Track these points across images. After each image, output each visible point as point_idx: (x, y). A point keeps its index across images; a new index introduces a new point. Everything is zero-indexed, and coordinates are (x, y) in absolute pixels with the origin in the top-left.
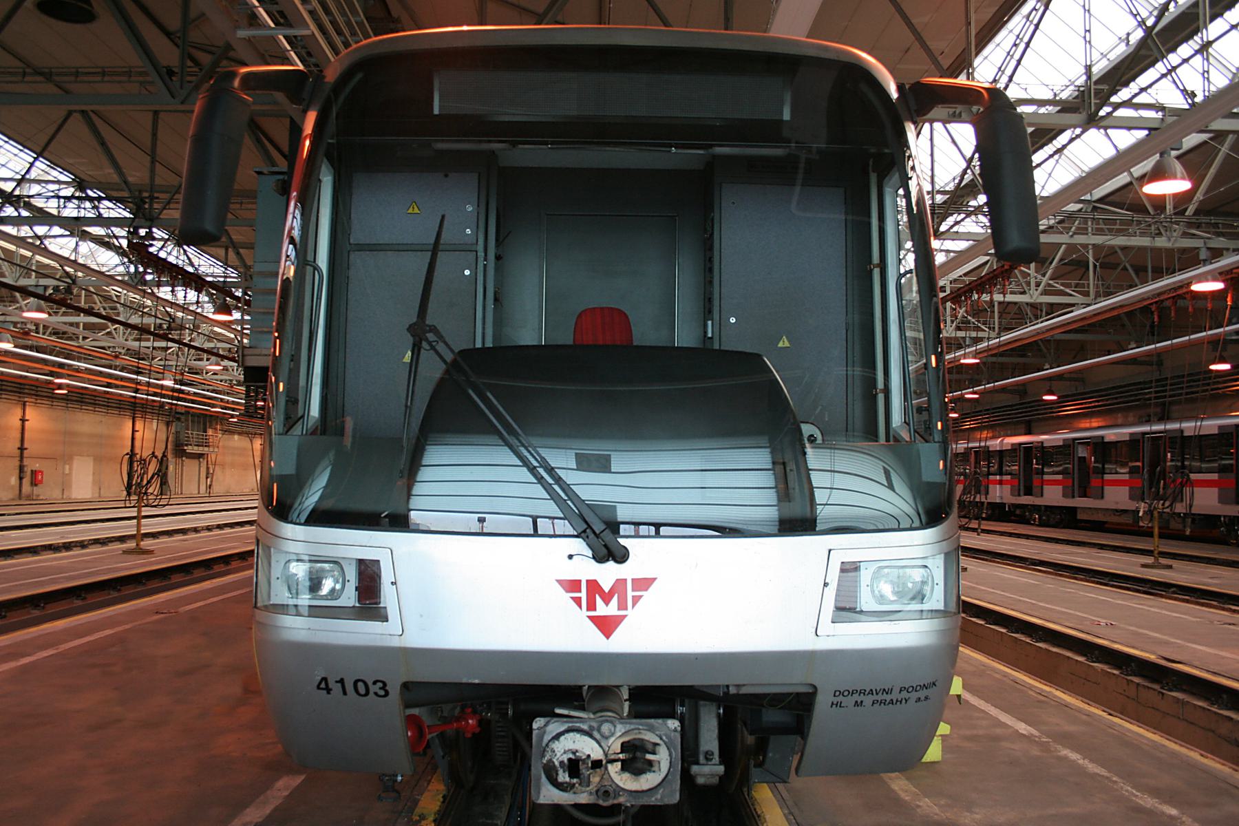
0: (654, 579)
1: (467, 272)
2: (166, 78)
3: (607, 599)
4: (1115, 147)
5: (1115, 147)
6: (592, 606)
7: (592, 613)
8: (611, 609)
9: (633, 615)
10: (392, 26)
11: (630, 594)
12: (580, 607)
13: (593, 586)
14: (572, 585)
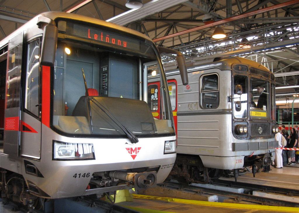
0: (43, 177)
2: (290, 166)
3: (134, 152)
6: (131, 153)
7: (132, 155)
10: (293, 84)
11: (137, 150)
12: (129, 153)
13: (132, 149)
14: (128, 149)
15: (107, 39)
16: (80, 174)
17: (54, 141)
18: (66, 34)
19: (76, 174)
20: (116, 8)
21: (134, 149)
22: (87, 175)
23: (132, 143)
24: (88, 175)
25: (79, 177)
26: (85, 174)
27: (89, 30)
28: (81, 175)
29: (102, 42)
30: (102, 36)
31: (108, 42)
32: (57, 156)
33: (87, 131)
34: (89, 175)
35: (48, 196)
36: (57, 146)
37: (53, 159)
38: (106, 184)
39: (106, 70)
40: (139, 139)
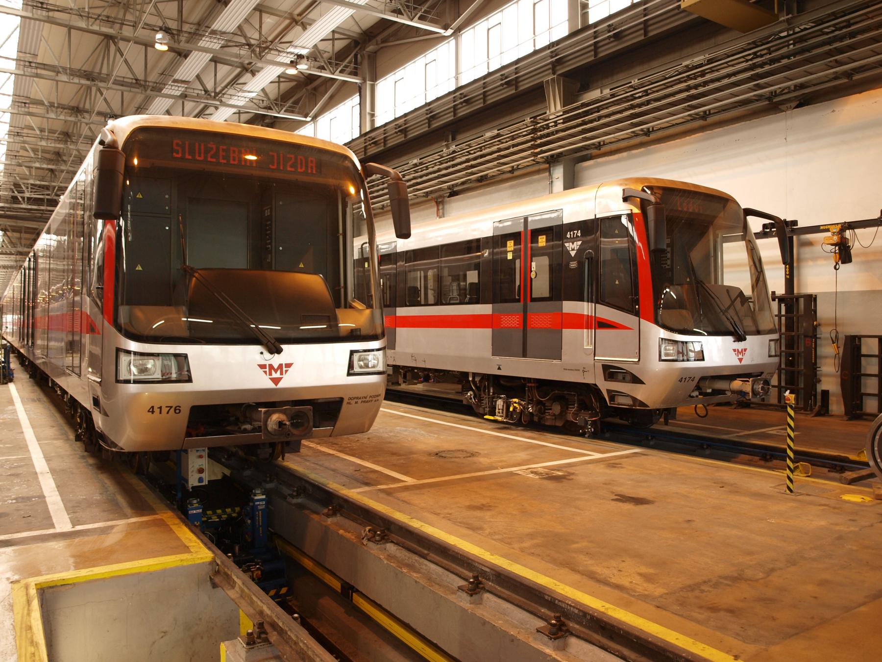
1: (167, 196)
3: (276, 371)
4: (13, 59)
5: (13, 59)
6: (270, 374)
8: (278, 375)
9: (286, 377)
11: (284, 369)
13: (271, 366)
14: (262, 367)
16: (160, 408)
17: (118, 350)
19: (153, 407)
20: (218, 65)
21: (276, 367)
23: (271, 352)
24: (177, 410)
32: (123, 376)
37: (118, 381)
40: (283, 346)
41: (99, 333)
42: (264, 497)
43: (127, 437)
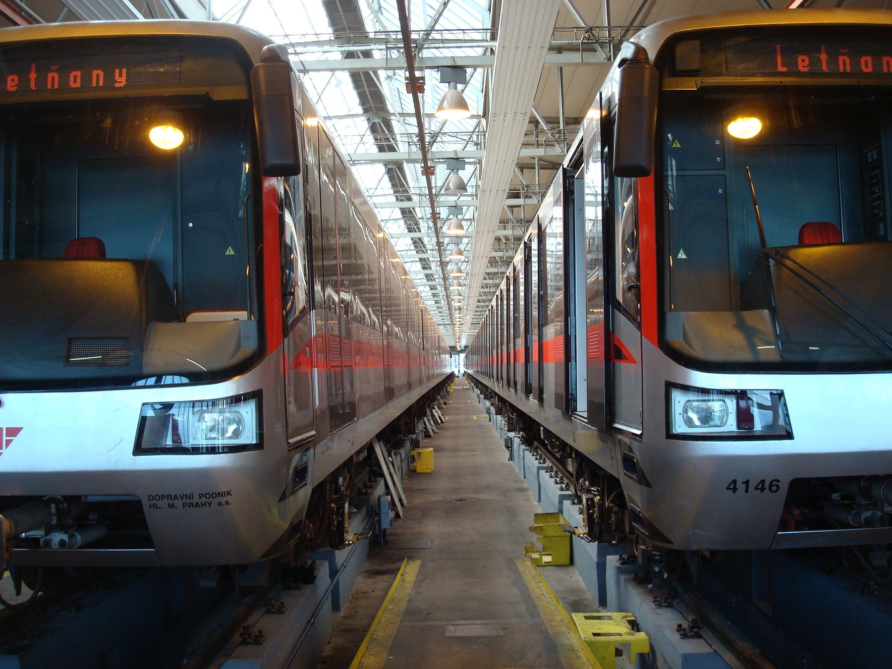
0: (22, 428)
15: (844, 61)
16: (747, 483)
18: (704, 76)
19: (734, 482)
22: (771, 485)
24: (774, 485)
25: (747, 491)
26: (763, 482)
27: (778, 46)
28: (752, 486)
29: (845, 74)
30: (824, 57)
31: (848, 70)
32: (680, 427)
33: (767, 350)
34: (778, 487)
35: (670, 542)
36: (679, 399)
37: (70, 341)
38: (866, 519)
39: (875, 157)
41: (635, 362)
42: (56, 87)
43: (694, 526)
